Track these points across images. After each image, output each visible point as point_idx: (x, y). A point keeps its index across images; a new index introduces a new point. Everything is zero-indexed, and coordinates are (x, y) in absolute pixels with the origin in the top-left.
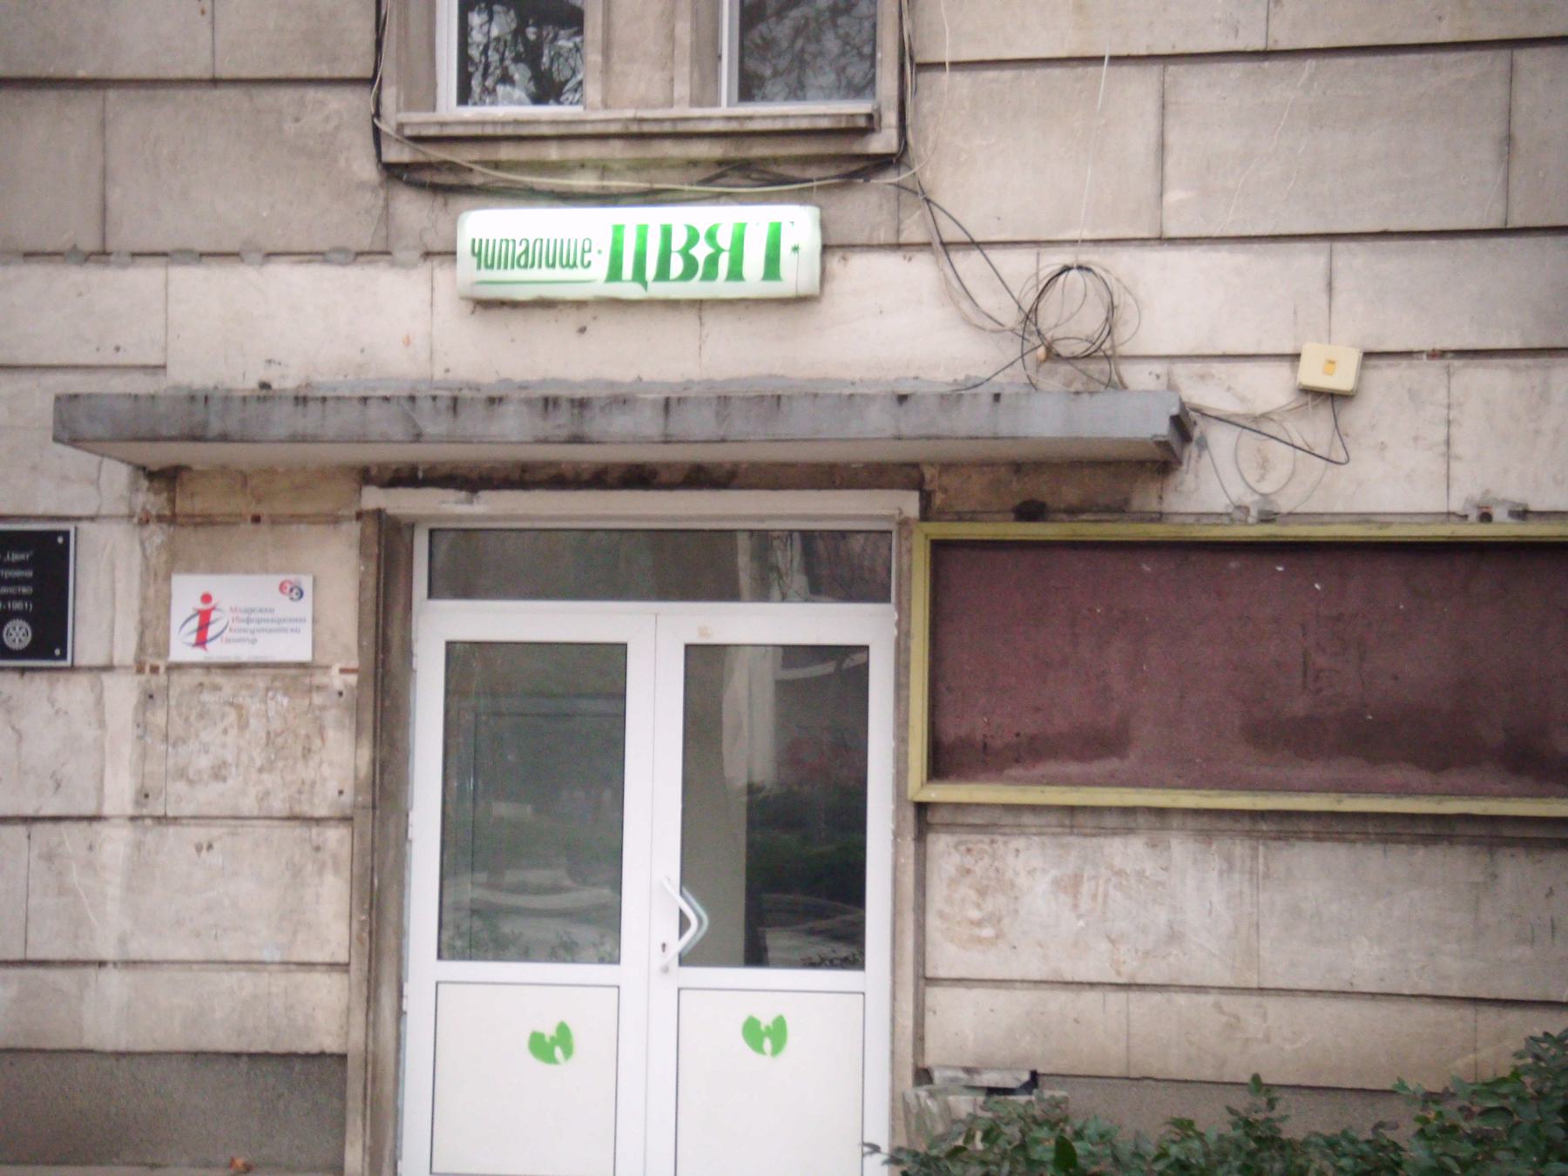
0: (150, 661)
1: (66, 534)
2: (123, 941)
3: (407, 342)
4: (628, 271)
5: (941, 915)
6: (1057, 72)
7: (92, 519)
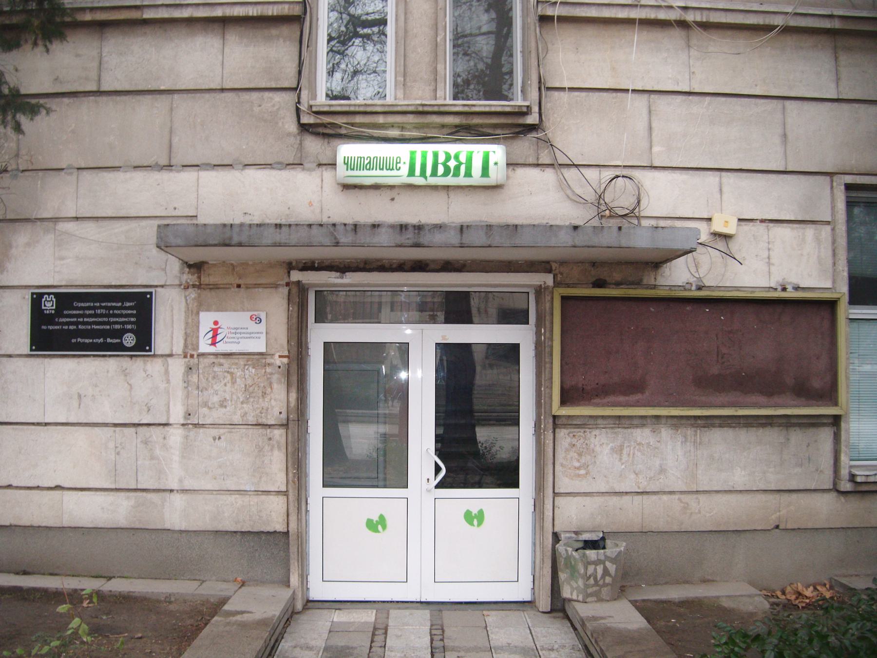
0: (190, 353)
1: (151, 293)
2: (181, 481)
3: (311, 204)
4: (418, 172)
5: (562, 465)
6: (605, 95)
7: (162, 286)
